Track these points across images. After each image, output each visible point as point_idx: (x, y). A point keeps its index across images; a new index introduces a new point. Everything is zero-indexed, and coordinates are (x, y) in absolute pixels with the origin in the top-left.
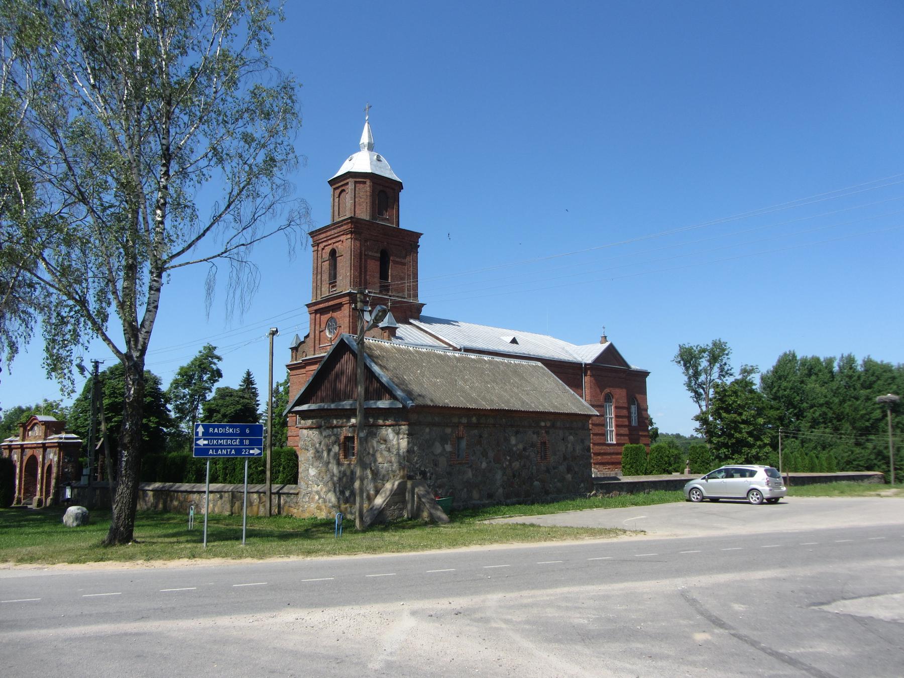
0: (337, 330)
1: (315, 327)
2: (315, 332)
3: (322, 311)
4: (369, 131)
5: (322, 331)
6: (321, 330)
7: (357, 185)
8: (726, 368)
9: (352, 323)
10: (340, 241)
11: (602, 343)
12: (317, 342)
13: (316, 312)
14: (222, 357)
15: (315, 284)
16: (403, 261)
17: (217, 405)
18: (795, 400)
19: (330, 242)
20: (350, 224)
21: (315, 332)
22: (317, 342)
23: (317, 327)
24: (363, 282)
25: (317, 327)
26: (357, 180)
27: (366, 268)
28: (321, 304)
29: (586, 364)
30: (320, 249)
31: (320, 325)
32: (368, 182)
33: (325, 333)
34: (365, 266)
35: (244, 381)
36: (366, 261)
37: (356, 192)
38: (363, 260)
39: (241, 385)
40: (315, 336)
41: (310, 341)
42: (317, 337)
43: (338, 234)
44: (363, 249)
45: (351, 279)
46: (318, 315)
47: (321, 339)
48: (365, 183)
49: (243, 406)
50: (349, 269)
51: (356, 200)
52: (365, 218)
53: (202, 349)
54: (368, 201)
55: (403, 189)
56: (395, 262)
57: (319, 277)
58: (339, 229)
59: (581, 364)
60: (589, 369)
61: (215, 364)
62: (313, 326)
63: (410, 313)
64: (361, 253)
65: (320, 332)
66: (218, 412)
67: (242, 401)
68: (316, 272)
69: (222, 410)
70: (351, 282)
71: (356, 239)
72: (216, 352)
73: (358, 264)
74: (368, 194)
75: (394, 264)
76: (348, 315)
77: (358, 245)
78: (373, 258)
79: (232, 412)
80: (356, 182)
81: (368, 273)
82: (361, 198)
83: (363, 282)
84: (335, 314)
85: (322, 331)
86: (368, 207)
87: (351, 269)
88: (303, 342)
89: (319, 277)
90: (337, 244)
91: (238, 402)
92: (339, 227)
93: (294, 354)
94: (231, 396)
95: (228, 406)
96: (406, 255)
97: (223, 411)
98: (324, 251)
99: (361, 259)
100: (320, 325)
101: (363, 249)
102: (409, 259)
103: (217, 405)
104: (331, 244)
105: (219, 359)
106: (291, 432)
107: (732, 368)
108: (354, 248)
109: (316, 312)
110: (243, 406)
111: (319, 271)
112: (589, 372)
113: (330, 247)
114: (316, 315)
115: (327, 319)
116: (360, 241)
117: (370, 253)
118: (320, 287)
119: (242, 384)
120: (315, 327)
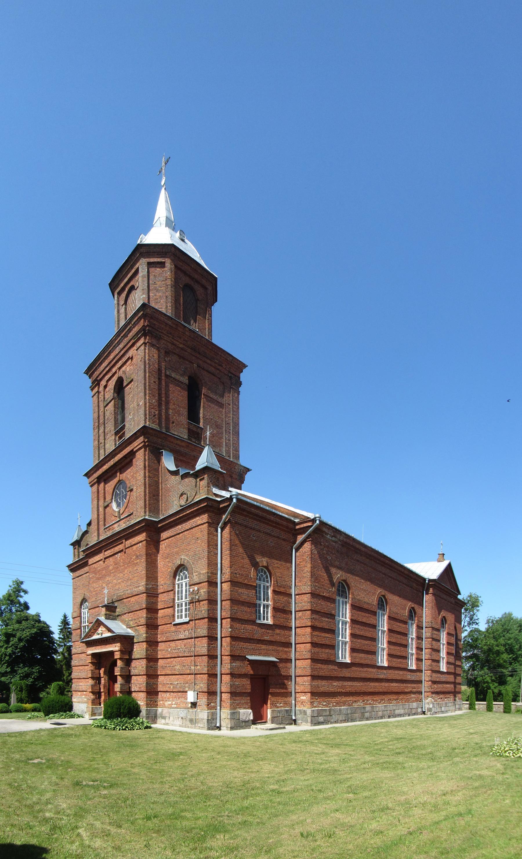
0: (128, 497)
1: (98, 502)
2: (98, 510)
3: (104, 478)
4: (166, 201)
5: (108, 506)
6: (106, 504)
7: (151, 270)
8: (475, 617)
9: (149, 477)
10: (129, 359)
11: (439, 561)
12: (101, 523)
13: (99, 480)
14: (29, 591)
15: (97, 442)
16: (220, 400)
17: (14, 630)
18: (515, 648)
19: (114, 370)
20: (142, 320)
21: (98, 510)
22: (101, 523)
23: (101, 503)
24: (164, 417)
25: (101, 503)
26: (152, 260)
27: (167, 396)
28: (104, 464)
29: (430, 580)
30: (101, 389)
31: (105, 498)
32: (168, 263)
33: (111, 507)
34: (166, 394)
35: (62, 623)
36: (167, 386)
37: (151, 282)
38: (163, 383)
39: (59, 626)
40: (98, 515)
41: (94, 527)
42: (101, 517)
43: (125, 349)
44: (163, 364)
45: (145, 411)
46: (102, 485)
47: (107, 517)
48: (162, 265)
49: (38, 630)
50: (142, 394)
51: (151, 294)
52: (163, 310)
53: (11, 584)
54: (169, 294)
55: (216, 301)
56: (209, 399)
57: (101, 430)
58: (126, 340)
59: (425, 579)
60: (432, 586)
61: (21, 597)
62: (95, 502)
63: (230, 479)
64: (160, 370)
65: (105, 507)
66: (14, 636)
67: (37, 624)
68: (97, 424)
69: (18, 634)
70: (145, 415)
71: (152, 345)
72: (23, 587)
73: (156, 387)
74: (169, 282)
75: (208, 400)
76: (142, 466)
77: (156, 356)
78: (178, 383)
79: (27, 636)
80: (150, 264)
81: (171, 406)
82: (157, 291)
83: (164, 417)
84: (124, 474)
85: (108, 506)
86: (169, 304)
87: (145, 394)
88: (86, 532)
89: (101, 430)
90: (123, 369)
91: (33, 627)
92: (126, 336)
93: (76, 551)
94: (27, 620)
95: (24, 630)
96: (224, 392)
97: (18, 635)
98: (107, 389)
99: (160, 379)
100: (105, 498)
101: (163, 364)
102: (228, 398)
103: (14, 630)
104: (116, 372)
105: (26, 592)
106: (76, 649)
107: (478, 619)
108: (149, 360)
109: (99, 480)
110: (38, 630)
111: (101, 421)
112: (431, 590)
113: (115, 378)
114: (99, 485)
115: (113, 487)
116: (158, 349)
117: (173, 375)
118: (103, 444)
119: (60, 625)
120: (98, 502)
